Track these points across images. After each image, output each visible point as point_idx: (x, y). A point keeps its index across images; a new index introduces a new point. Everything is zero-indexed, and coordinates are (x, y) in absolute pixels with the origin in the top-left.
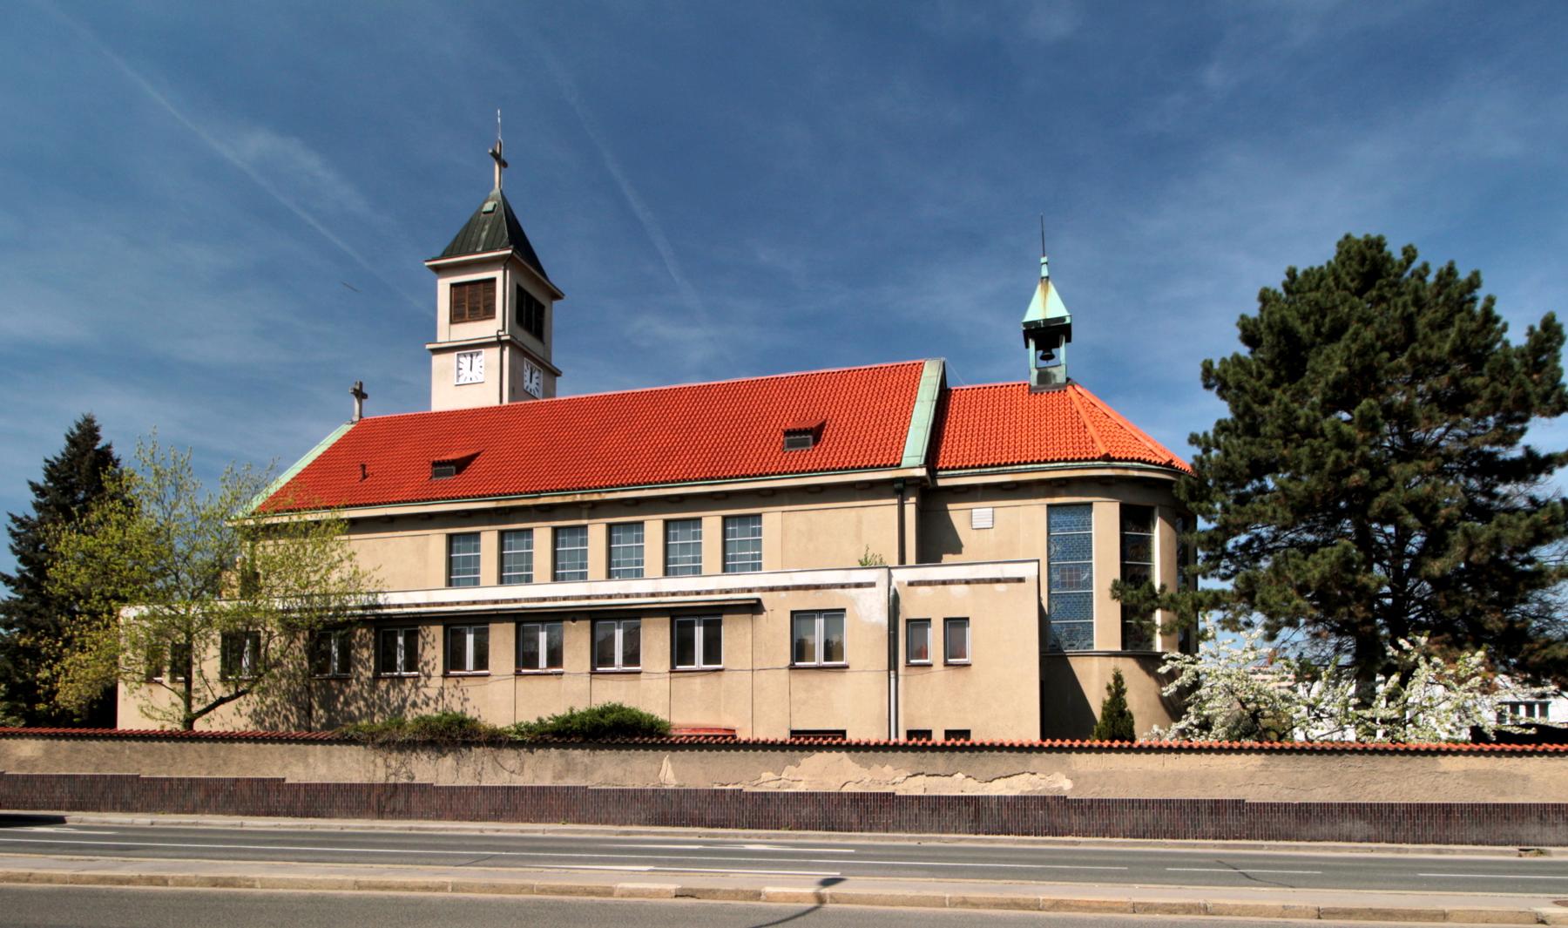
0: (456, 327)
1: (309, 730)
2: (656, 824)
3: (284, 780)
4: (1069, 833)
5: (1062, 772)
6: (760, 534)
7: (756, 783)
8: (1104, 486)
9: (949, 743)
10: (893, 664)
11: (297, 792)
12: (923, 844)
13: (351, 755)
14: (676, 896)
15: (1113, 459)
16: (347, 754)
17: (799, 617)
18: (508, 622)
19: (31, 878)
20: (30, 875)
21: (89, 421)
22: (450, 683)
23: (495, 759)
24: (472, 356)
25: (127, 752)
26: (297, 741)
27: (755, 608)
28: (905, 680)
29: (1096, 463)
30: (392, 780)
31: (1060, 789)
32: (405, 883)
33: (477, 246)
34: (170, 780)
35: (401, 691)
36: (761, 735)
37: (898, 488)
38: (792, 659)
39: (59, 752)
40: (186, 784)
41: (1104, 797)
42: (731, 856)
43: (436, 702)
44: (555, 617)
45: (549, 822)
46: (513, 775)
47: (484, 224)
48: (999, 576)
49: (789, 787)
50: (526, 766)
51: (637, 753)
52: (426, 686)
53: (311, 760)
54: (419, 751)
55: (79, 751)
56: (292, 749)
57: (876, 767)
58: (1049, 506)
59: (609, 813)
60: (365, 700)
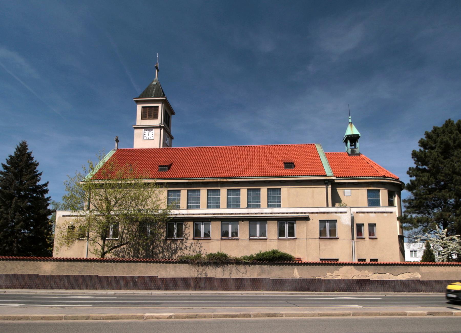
0: (143, 121)
1: (138, 257)
3: (157, 276)
4: (421, 291)
5: (418, 272)
6: (180, 196)
7: (325, 276)
8: (383, 185)
9: (371, 263)
10: (353, 238)
12: (387, 296)
13: (183, 267)
14: (427, 315)
15: (385, 177)
16: (182, 267)
18: (218, 221)
19: (197, 316)
20: (197, 315)
22: (195, 241)
23: (237, 268)
24: (149, 131)
25: (93, 266)
26: (134, 262)
27: (307, 219)
28: (357, 243)
29: (381, 178)
30: (199, 276)
31: (418, 277)
32: (336, 313)
33: (152, 95)
35: (176, 244)
36: (310, 260)
37: (326, 182)
38: (221, 236)
39: (63, 267)
40: (118, 279)
41: (430, 280)
42: (89, 301)
43: (190, 248)
44: (207, 220)
45: (257, 291)
46: (243, 274)
47: (153, 88)
49: (336, 278)
50: (248, 271)
51: (286, 266)
52: (186, 242)
53: (168, 269)
54: (209, 266)
55: (72, 266)
56: (161, 265)
57: (363, 271)
60: (161, 247)
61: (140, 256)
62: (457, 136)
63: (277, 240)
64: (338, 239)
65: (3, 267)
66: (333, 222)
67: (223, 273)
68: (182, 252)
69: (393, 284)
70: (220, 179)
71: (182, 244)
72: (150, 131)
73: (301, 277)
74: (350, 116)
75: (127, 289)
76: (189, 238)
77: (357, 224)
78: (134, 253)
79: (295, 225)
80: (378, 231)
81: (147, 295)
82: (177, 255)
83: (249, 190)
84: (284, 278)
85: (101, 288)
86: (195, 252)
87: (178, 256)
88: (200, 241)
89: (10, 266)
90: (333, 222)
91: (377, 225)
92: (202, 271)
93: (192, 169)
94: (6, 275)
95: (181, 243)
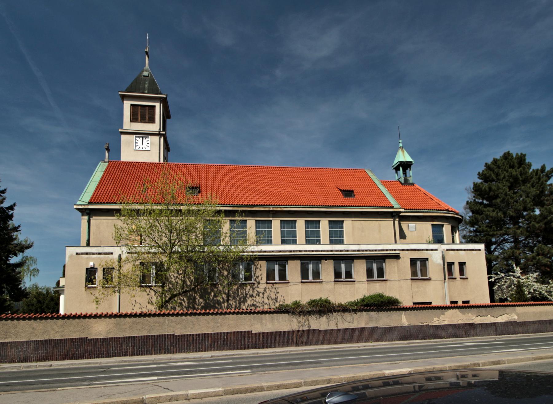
1: (194, 308)
3: (252, 331)
7: (433, 322)
10: (445, 279)
11: (259, 336)
17: (413, 261)
18: (296, 260)
23: (342, 317)
25: (167, 322)
27: (397, 257)
30: (301, 329)
31: (515, 319)
34: (192, 335)
39: (125, 325)
43: (263, 294)
45: (365, 342)
46: (350, 324)
47: (145, 81)
48: (473, 248)
49: (442, 323)
52: (258, 287)
53: (264, 321)
54: (312, 315)
55: (137, 323)
58: (306, 221)
59: (386, 337)
60: (225, 293)
61: (196, 306)
62: (524, 170)
63: (367, 282)
64: (429, 279)
65: (31, 329)
66: (424, 261)
68: (253, 300)
69: (495, 327)
70: (273, 207)
71: (253, 289)
72: (144, 139)
73: (410, 323)
74: (400, 140)
75: (214, 351)
76: (261, 282)
77: (448, 263)
78: (188, 303)
79: (287, 266)
80: (468, 269)
81: (252, 355)
82: (246, 304)
83: (282, 222)
84: (393, 326)
85: (180, 351)
86: (270, 299)
87: (249, 305)
88: (276, 286)
90: (424, 261)
91: (467, 264)
92: (305, 322)
93: (100, 192)
95: (251, 288)
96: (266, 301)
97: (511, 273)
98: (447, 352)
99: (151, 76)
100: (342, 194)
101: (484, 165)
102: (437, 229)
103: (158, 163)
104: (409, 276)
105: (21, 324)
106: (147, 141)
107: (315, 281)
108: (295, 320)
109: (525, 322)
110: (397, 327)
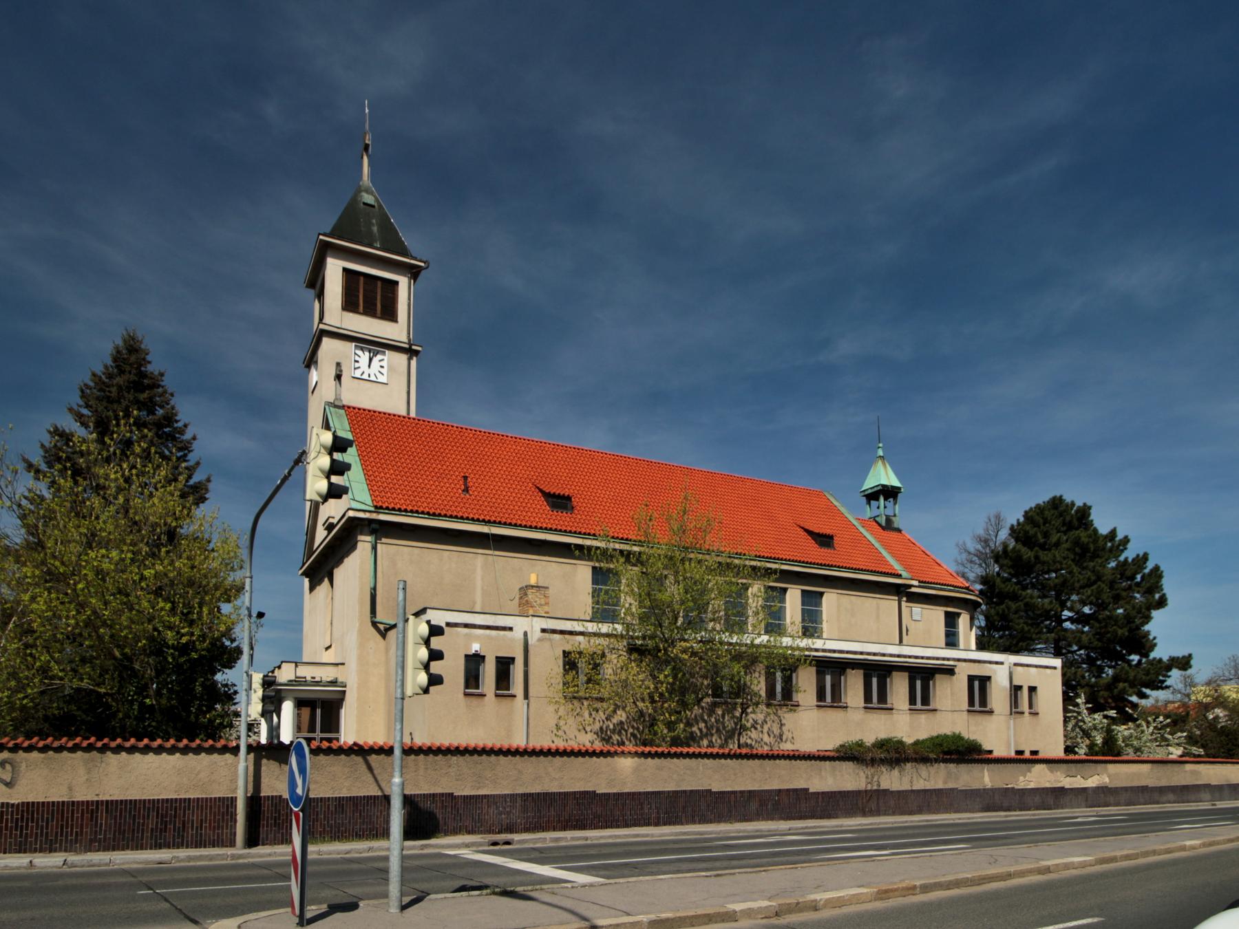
2: (986, 811)
10: (1011, 714)
17: (971, 679)
21: (1156, 565)
25: (701, 768)
27: (950, 671)
30: (869, 787)
34: (734, 792)
39: (646, 770)
53: (823, 773)
58: (803, 591)
60: (705, 722)
64: (991, 712)
67: (901, 779)
85: (719, 819)
86: (772, 736)
89: (530, 770)
90: (985, 681)
94: (524, 795)
96: (766, 739)
97: (1071, 708)
98: (1083, 830)
99: (380, 206)
100: (813, 539)
101: (1023, 513)
102: (951, 620)
103: (404, 417)
104: (965, 706)
105: (502, 762)
106: (380, 361)
107: (835, 704)
108: (862, 774)
109: (1117, 788)
110: (979, 790)
